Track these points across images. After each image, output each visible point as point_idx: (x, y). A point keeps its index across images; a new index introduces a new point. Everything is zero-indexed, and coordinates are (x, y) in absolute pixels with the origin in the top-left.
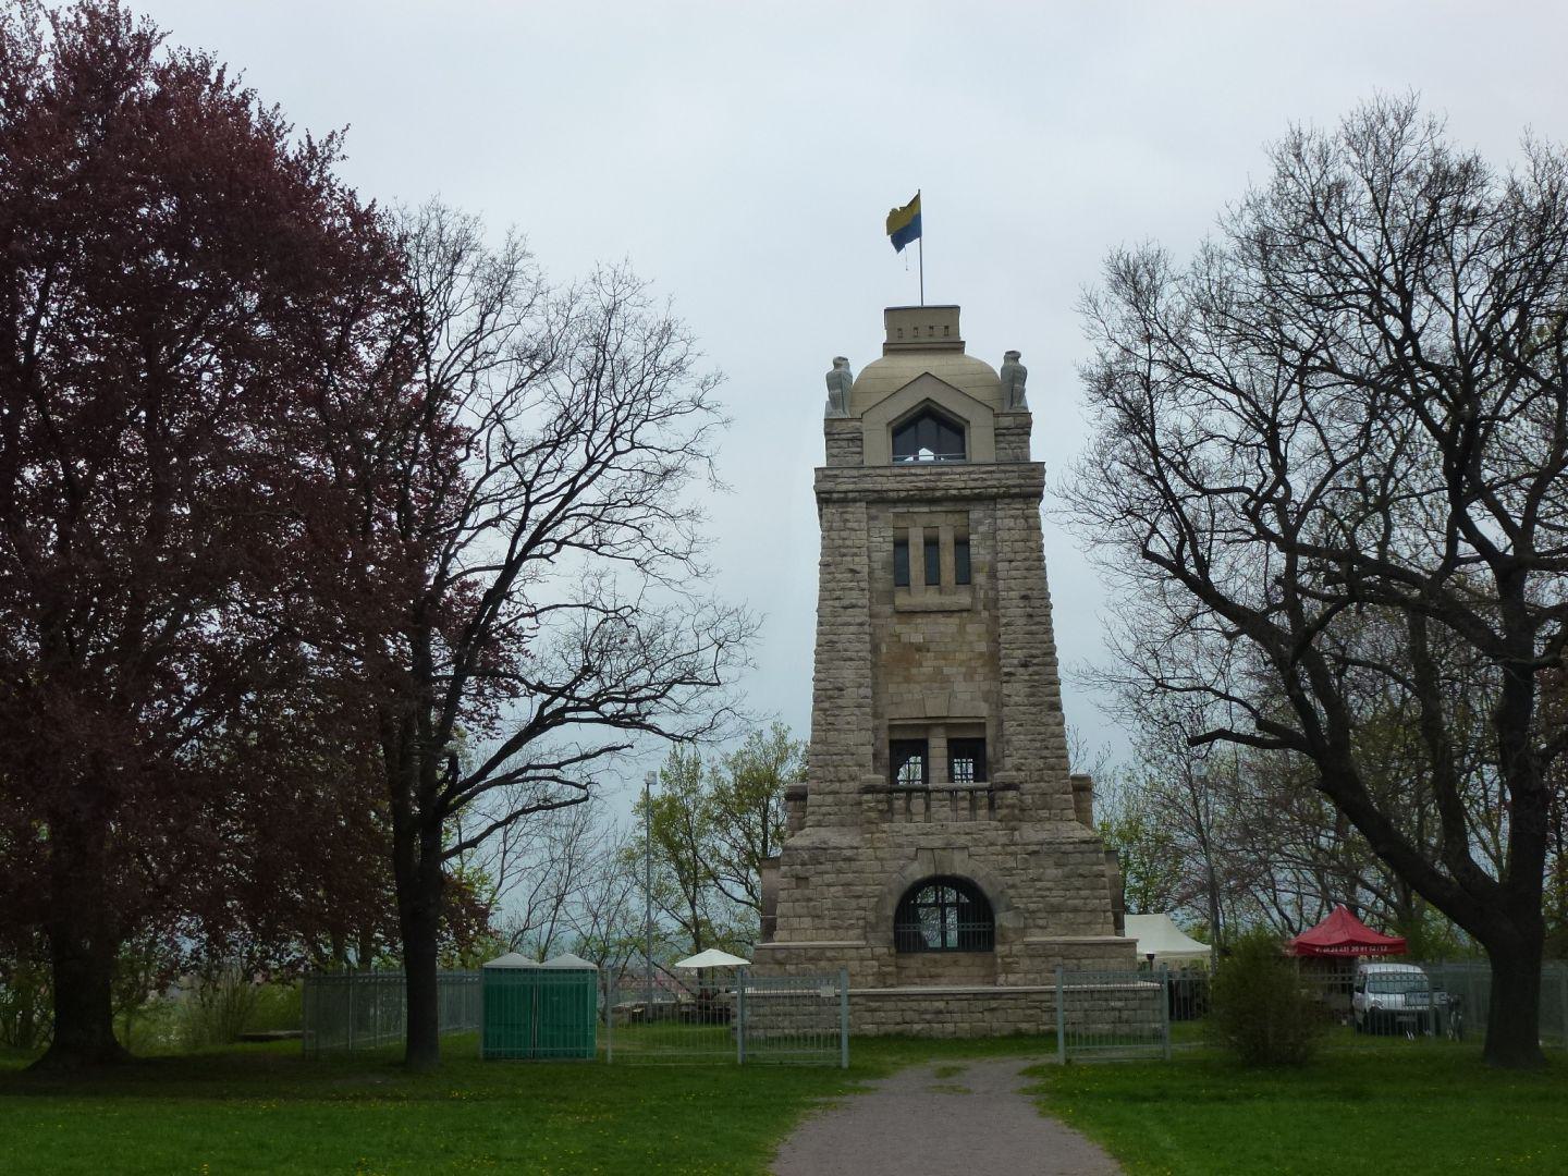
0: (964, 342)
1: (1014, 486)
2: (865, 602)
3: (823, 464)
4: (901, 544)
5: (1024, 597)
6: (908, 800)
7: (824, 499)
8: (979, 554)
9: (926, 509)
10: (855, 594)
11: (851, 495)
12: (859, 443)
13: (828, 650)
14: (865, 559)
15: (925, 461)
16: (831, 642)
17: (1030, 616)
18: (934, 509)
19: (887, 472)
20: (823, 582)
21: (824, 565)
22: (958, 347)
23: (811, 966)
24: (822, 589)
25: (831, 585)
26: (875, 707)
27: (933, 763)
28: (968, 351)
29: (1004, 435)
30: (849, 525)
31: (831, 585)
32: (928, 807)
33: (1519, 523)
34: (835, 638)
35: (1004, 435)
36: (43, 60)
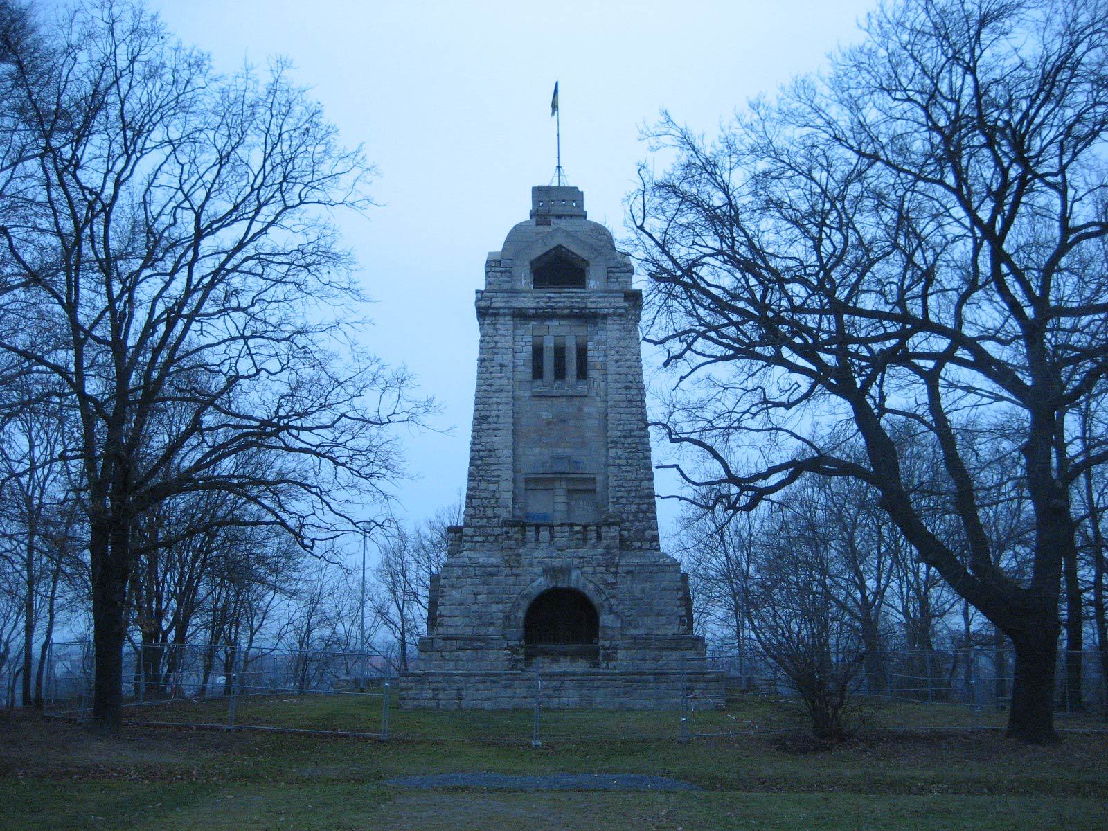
0: (582, 193)
1: (621, 308)
2: (510, 387)
3: (483, 288)
4: (538, 351)
5: (626, 388)
6: (537, 531)
7: (482, 313)
8: (594, 356)
9: (557, 323)
10: (504, 382)
11: (501, 311)
12: (508, 275)
13: (482, 421)
14: (510, 357)
15: (554, 278)
16: (485, 416)
17: (630, 401)
18: (562, 323)
19: (530, 295)
20: (480, 373)
21: (481, 362)
22: (584, 215)
23: (461, 654)
24: (479, 378)
25: (485, 376)
26: (514, 464)
27: (965, 370)
28: (588, 218)
29: (613, 272)
30: (500, 332)
31: (485, 376)
32: (552, 537)
33: (1038, 293)
34: (487, 414)
35: (613, 272)
36: (560, 450)
